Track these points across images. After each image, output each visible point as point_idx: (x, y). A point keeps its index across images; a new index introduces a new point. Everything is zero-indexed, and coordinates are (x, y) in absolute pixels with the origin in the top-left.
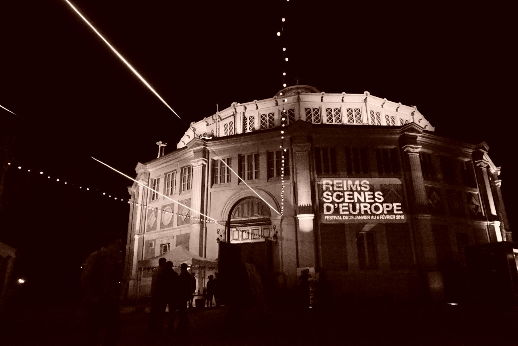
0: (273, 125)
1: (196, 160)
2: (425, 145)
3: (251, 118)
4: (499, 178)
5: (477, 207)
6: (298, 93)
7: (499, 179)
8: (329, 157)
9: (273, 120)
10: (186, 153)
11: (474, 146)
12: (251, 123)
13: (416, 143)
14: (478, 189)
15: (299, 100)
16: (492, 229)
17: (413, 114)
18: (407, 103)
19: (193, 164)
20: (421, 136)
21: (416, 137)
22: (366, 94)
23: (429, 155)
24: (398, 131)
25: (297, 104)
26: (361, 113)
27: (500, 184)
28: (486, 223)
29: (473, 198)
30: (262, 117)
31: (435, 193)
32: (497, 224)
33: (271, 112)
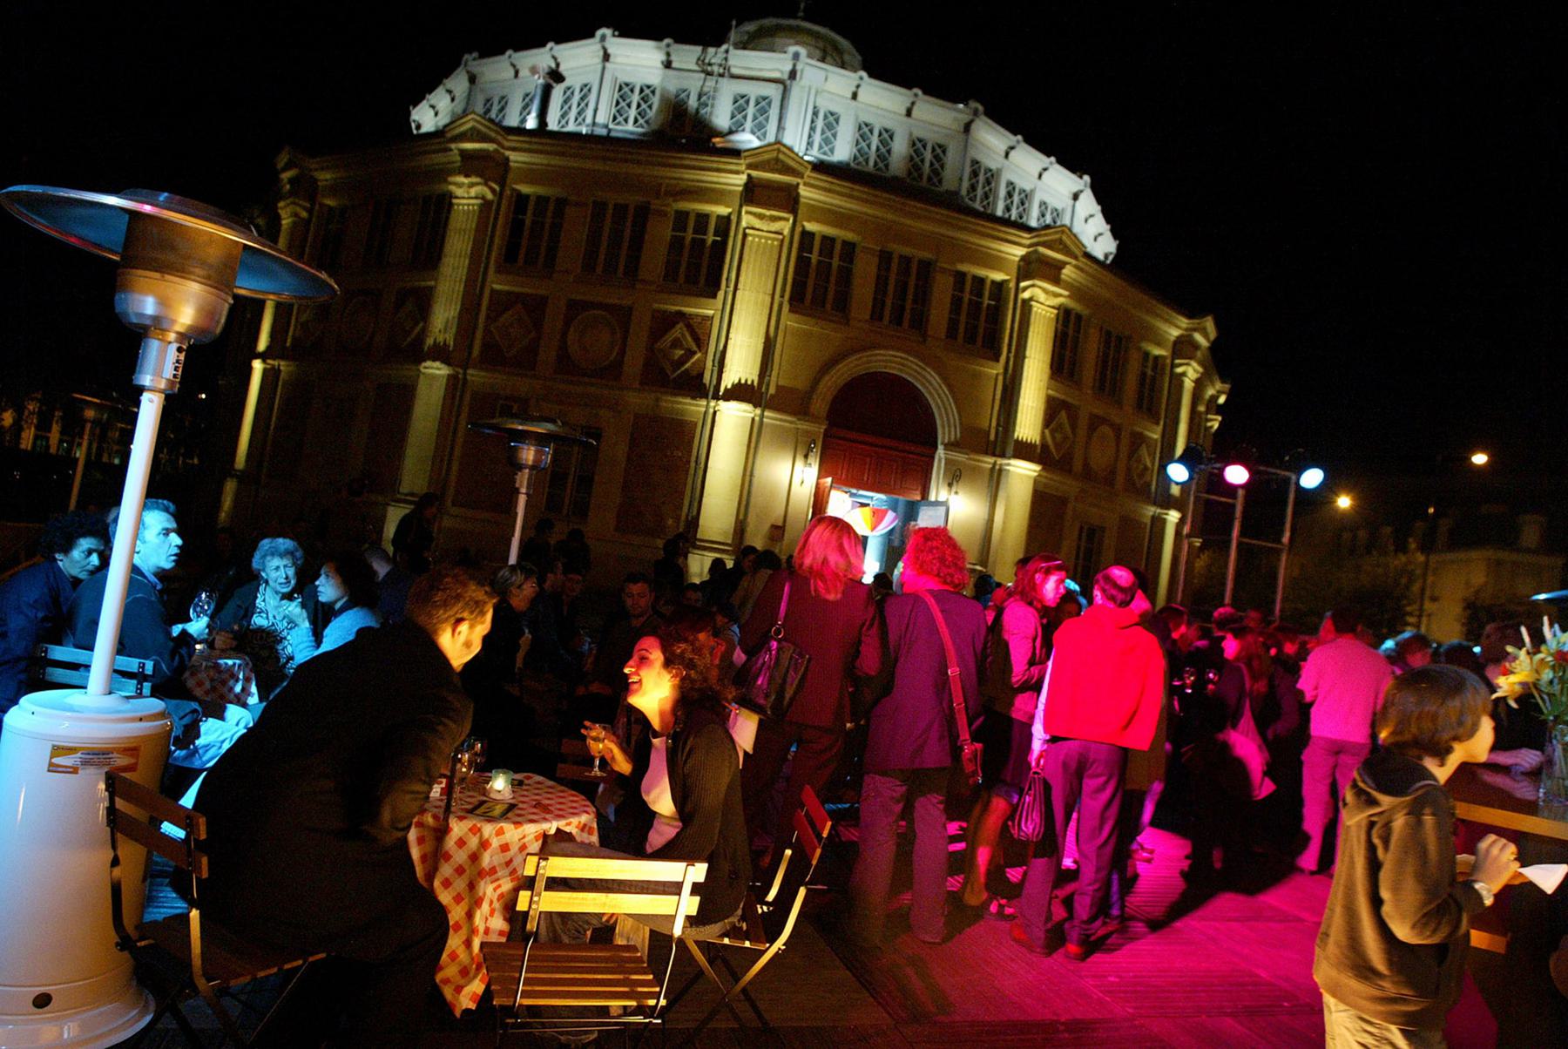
0: (887, 166)
1: (768, 213)
2: (1077, 292)
3: (626, 89)
4: (1220, 410)
5: (1146, 468)
6: (976, 113)
7: (1217, 413)
8: (624, 252)
9: (889, 151)
10: (426, 153)
11: (1184, 322)
12: (623, 104)
13: (1056, 281)
14: (1160, 429)
15: (967, 128)
16: (1159, 523)
17: (1076, 197)
18: (1072, 164)
19: (459, 192)
20: (1076, 267)
21: (1063, 265)
22: (796, 56)
23: (1079, 317)
24: (1026, 239)
25: (963, 136)
26: (616, 96)
27: (1216, 425)
28: (1152, 510)
29: (1144, 447)
30: (621, 89)
31: (1063, 414)
32: (1173, 516)
33: (649, 82)
